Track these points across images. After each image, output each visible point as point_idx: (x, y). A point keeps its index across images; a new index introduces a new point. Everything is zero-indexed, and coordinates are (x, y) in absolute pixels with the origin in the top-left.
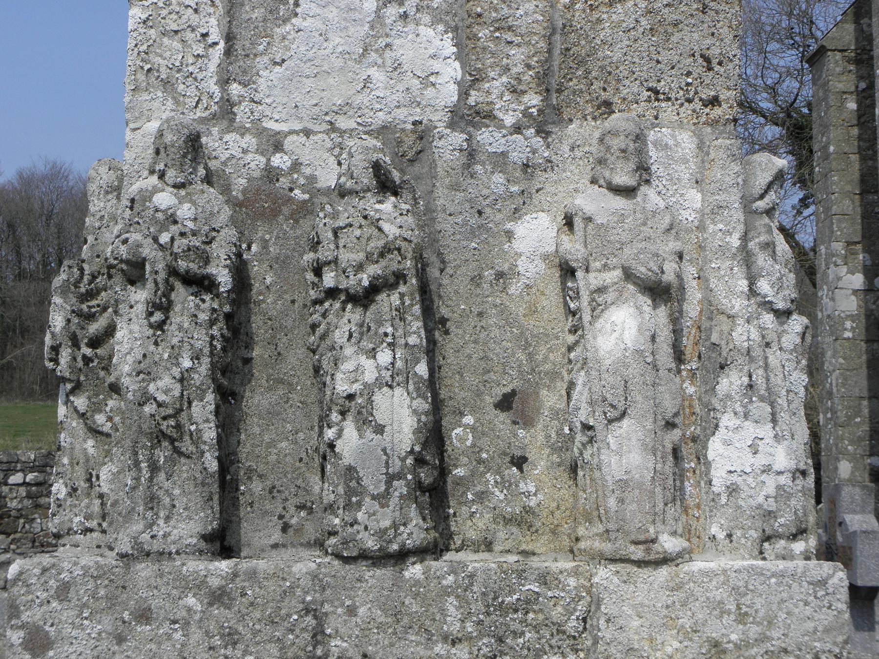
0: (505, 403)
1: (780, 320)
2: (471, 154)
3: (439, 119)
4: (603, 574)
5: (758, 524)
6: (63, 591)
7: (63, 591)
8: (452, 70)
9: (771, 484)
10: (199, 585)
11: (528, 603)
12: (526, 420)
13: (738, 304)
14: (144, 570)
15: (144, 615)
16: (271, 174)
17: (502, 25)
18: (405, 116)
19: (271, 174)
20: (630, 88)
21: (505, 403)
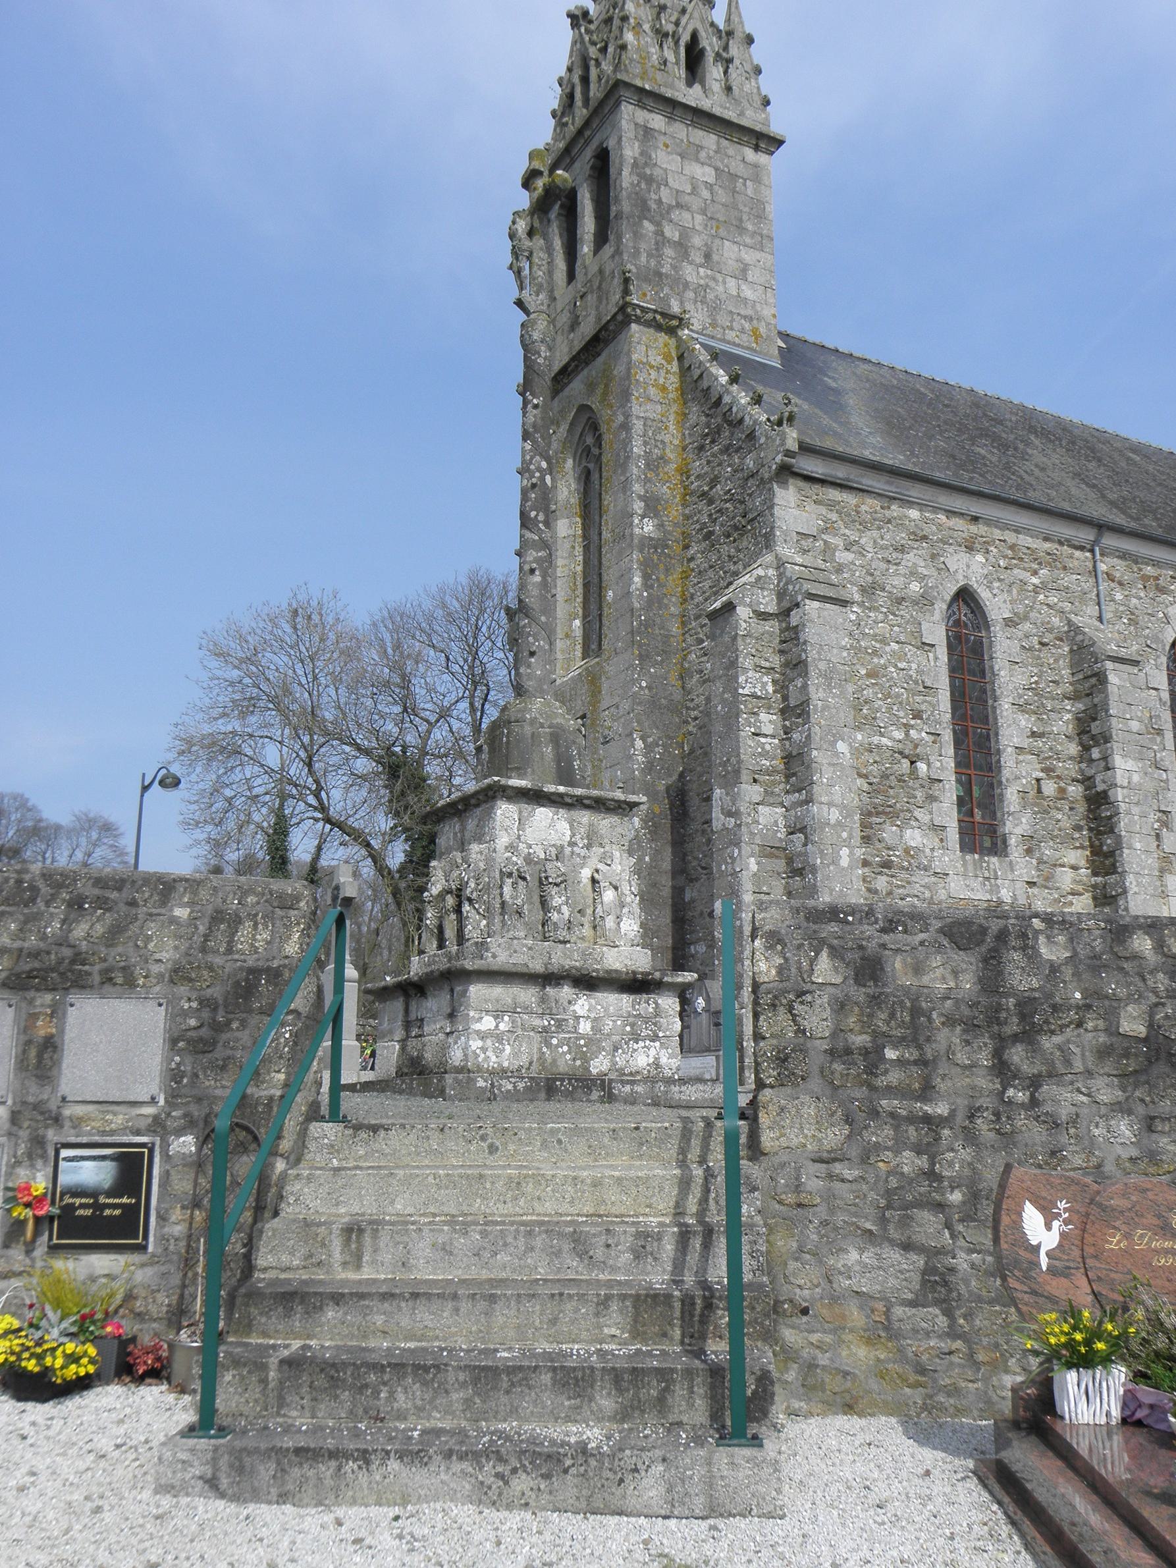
0: (579, 912)
1: (959, 770)
2: (573, 853)
3: (566, 844)
4: (605, 949)
5: (1010, 607)
6: (499, 945)
7: (499, 945)
8: (569, 832)
9: (633, 933)
10: (526, 946)
11: (590, 954)
12: (583, 916)
13: (628, 892)
14: (515, 941)
15: (515, 952)
16: (529, 854)
17: (579, 823)
18: (559, 843)
19: (529, 854)
20: (606, 840)
21: (579, 912)
